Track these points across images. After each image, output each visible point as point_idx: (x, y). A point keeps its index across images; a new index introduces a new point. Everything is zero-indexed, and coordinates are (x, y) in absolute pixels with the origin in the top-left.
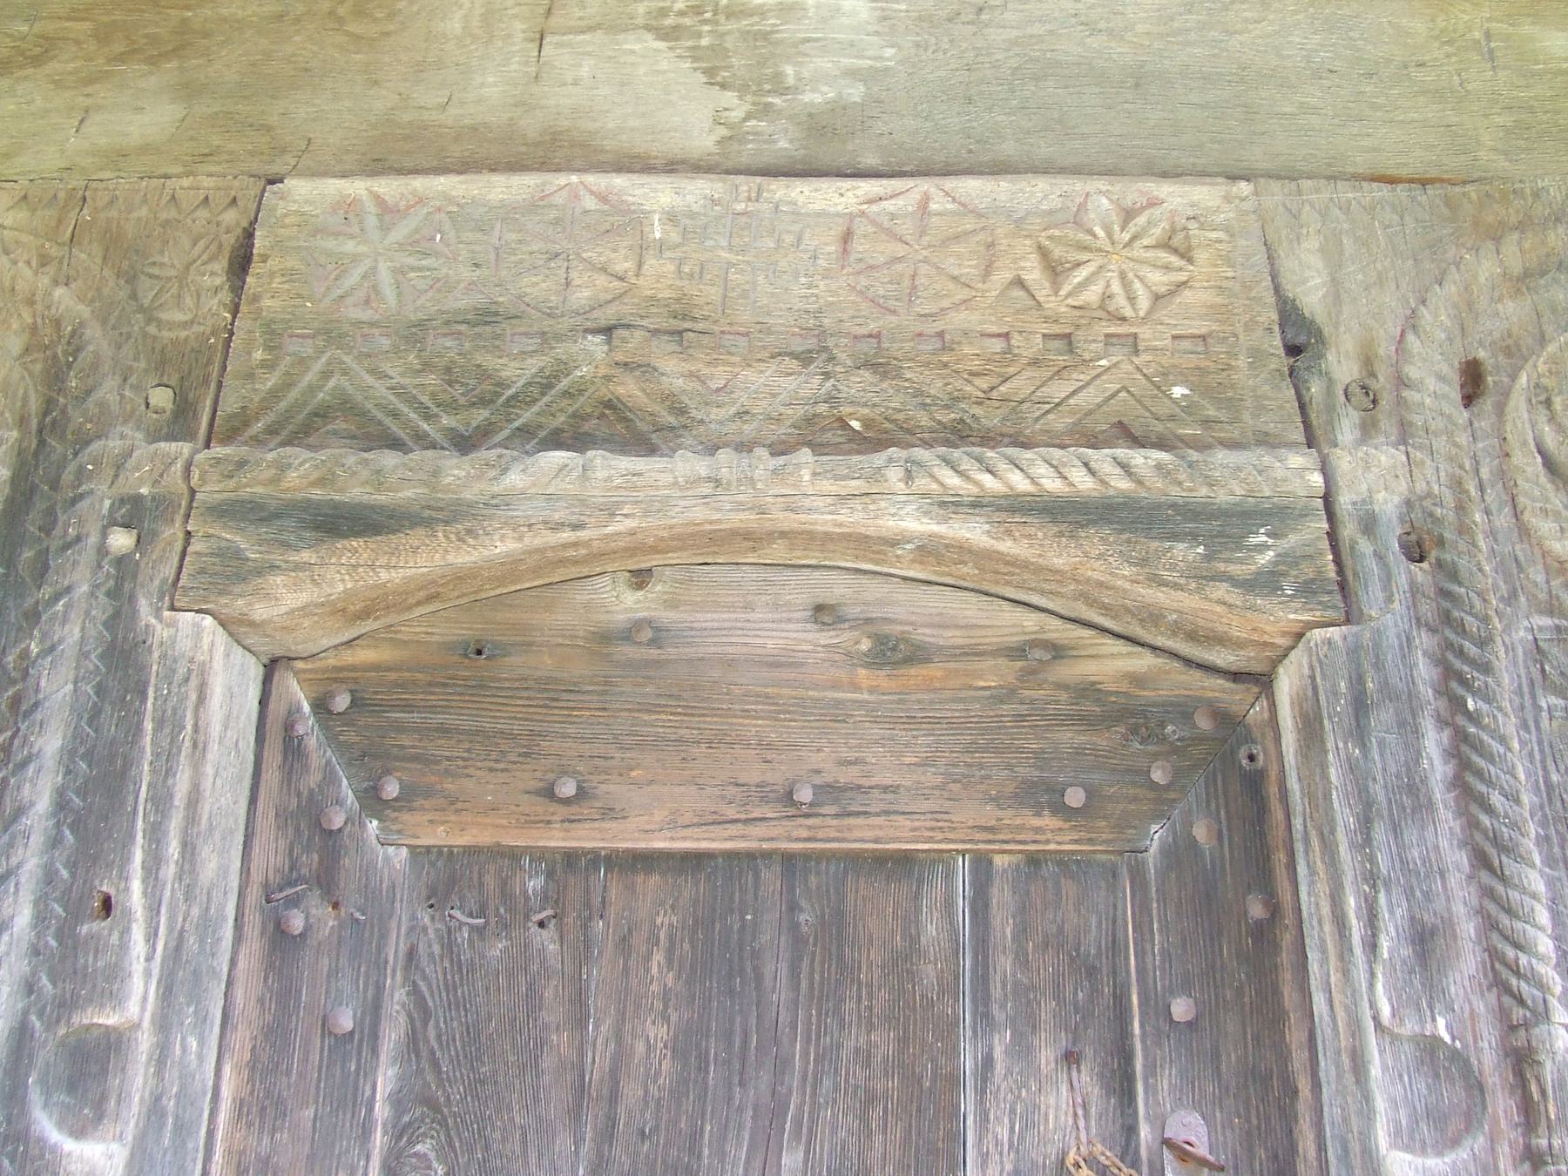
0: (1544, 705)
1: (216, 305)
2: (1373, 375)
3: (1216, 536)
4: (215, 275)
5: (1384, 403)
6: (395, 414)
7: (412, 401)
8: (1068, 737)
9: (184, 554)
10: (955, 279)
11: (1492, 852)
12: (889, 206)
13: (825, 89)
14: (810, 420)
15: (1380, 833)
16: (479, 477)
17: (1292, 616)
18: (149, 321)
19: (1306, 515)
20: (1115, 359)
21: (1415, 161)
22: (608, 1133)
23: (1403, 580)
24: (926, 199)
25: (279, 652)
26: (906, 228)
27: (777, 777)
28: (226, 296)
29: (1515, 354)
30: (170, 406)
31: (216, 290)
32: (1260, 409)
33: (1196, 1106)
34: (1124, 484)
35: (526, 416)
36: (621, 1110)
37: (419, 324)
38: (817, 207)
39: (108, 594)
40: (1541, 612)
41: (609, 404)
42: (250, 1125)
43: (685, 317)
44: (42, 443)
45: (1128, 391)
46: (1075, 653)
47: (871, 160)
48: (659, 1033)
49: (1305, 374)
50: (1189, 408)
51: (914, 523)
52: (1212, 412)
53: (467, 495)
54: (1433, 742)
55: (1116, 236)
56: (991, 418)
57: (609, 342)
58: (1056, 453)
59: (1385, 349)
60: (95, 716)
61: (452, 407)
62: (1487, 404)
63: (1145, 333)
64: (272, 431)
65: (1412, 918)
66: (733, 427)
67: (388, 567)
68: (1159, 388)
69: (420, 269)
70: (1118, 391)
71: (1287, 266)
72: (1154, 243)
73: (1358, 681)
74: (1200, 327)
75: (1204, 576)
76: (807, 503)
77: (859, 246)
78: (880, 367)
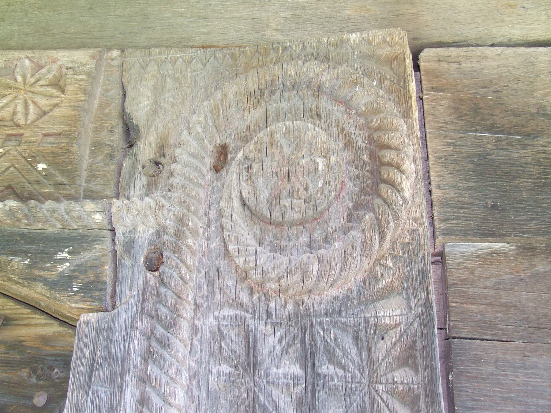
0: (215, 371)
2: (162, 155)
3: (39, 253)
17: (73, 305)
19: (96, 240)
20: (7, 148)
40: (231, 306)
45: (15, 168)
46: (16, 323)
50: (47, 175)
52: (60, 179)
63: (27, 133)
68: (31, 164)
70: (10, 167)
72: (47, 83)
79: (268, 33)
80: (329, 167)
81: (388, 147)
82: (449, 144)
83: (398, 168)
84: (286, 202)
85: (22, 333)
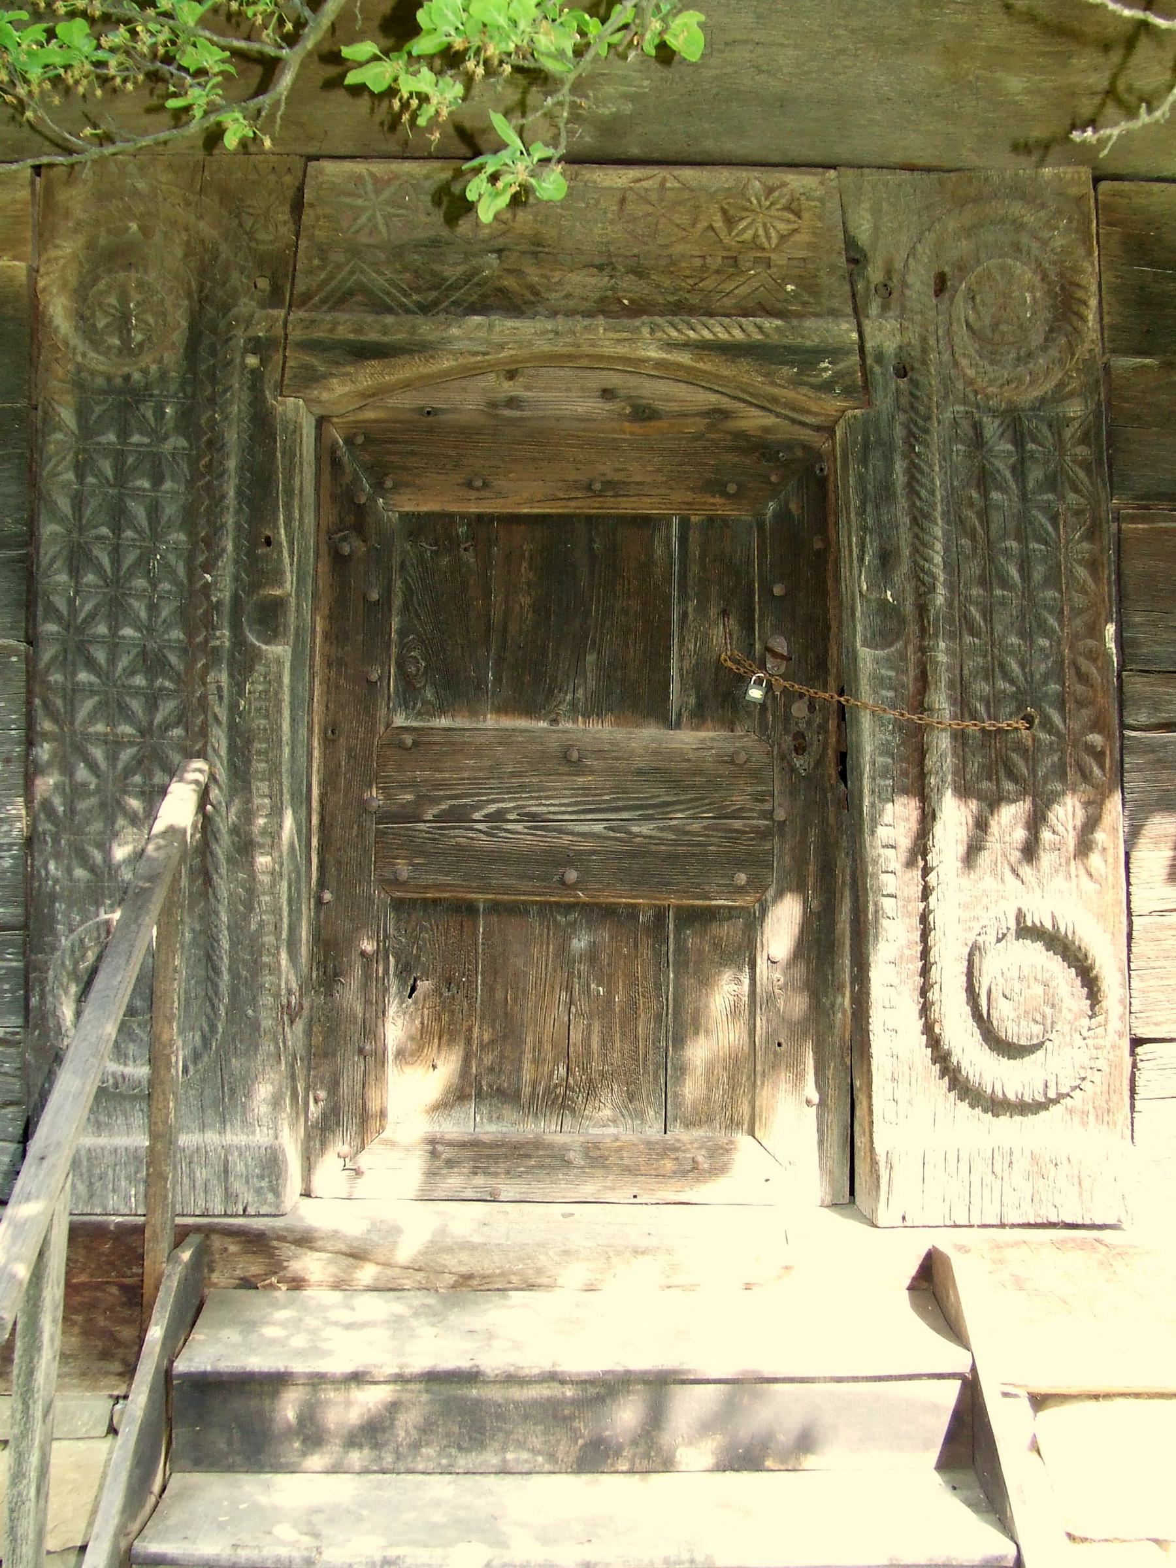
1: (286, 231)
2: (890, 279)
4: (283, 215)
5: (895, 295)
6: (388, 294)
7: (397, 287)
8: (732, 458)
9: (283, 369)
10: (678, 226)
11: (919, 517)
12: (645, 184)
13: (610, 105)
14: (603, 300)
15: (869, 508)
16: (436, 330)
18: (251, 239)
21: (926, 157)
22: (503, 646)
23: (893, 387)
24: (664, 181)
25: (324, 413)
26: (654, 197)
27: (583, 477)
28: (291, 226)
29: (962, 268)
30: (268, 288)
31: (285, 223)
32: (831, 296)
33: (783, 634)
34: (759, 337)
35: (456, 296)
36: (509, 637)
37: (401, 247)
38: (606, 184)
39: (249, 388)
41: (500, 290)
42: (331, 643)
43: (539, 245)
44: (201, 307)
47: (635, 151)
48: (526, 601)
49: (856, 278)
50: (796, 295)
51: (654, 353)
52: (806, 298)
53: (430, 338)
54: (899, 466)
55: (763, 203)
56: (695, 300)
57: (499, 258)
58: (726, 320)
59: (899, 265)
60: (251, 449)
61: (418, 290)
62: (946, 296)
63: (773, 256)
64: (324, 301)
65: (881, 548)
66: (564, 302)
67: (389, 374)
69: (398, 216)
71: (852, 218)
73: (866, 438)
74: (802, 254)
75: (796, 383)
76: (601, 343)
77: (630, 207)
78: (639, 272)
79: (965, 153)
80: (1034, 298)
81: (1078, 285)
82: (1117, 277)
83: (1085, 304)
84: (1004, 328)
85: (743, 424)
